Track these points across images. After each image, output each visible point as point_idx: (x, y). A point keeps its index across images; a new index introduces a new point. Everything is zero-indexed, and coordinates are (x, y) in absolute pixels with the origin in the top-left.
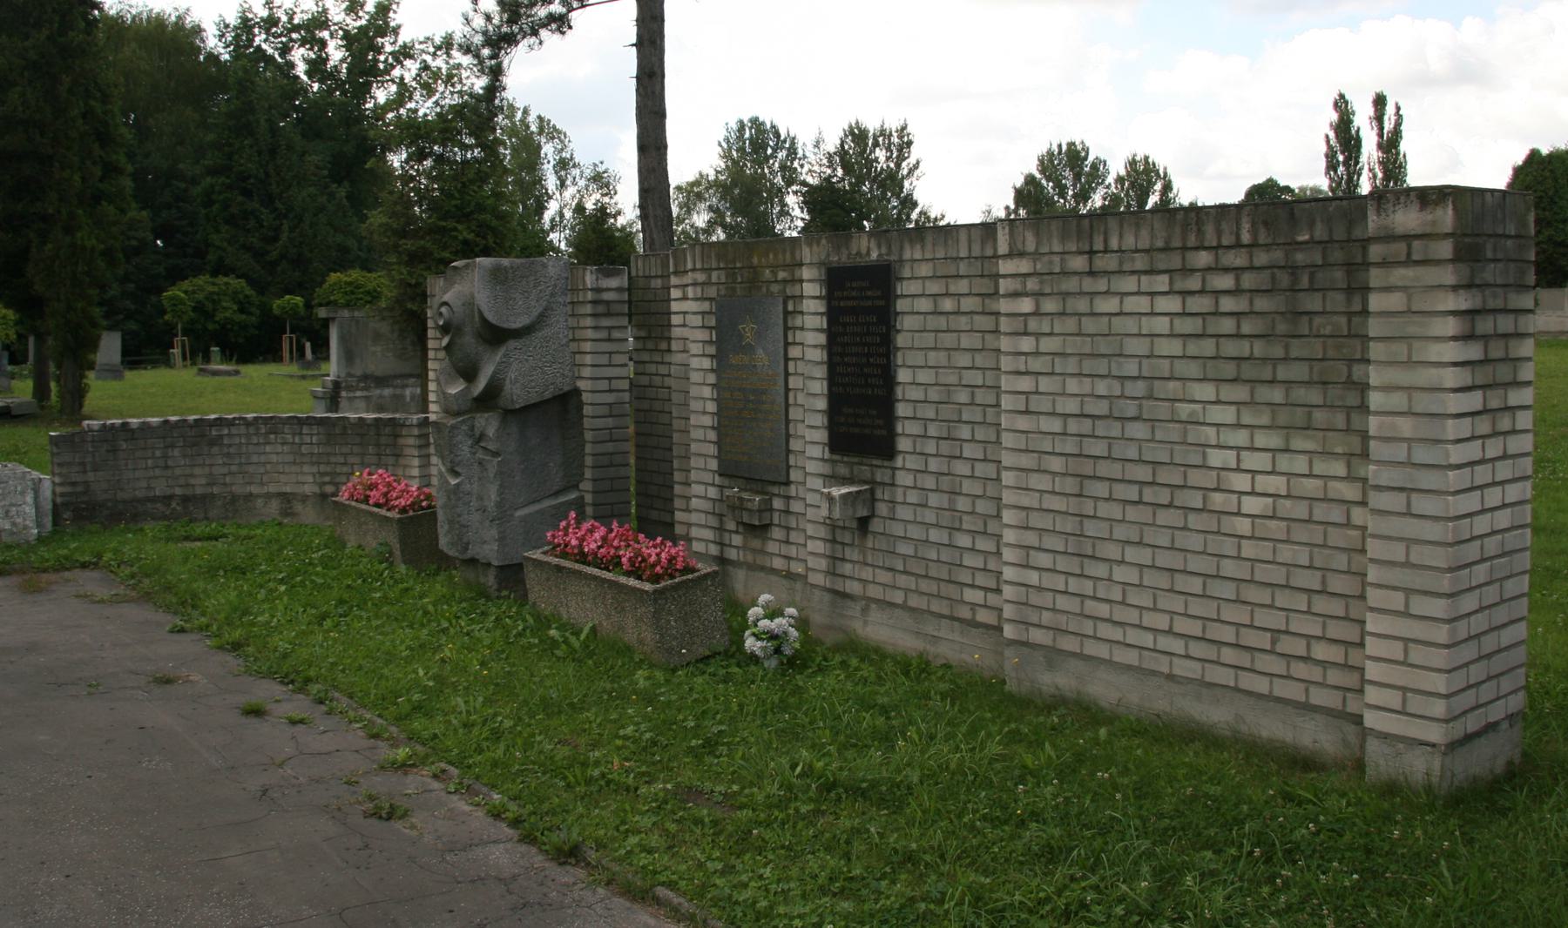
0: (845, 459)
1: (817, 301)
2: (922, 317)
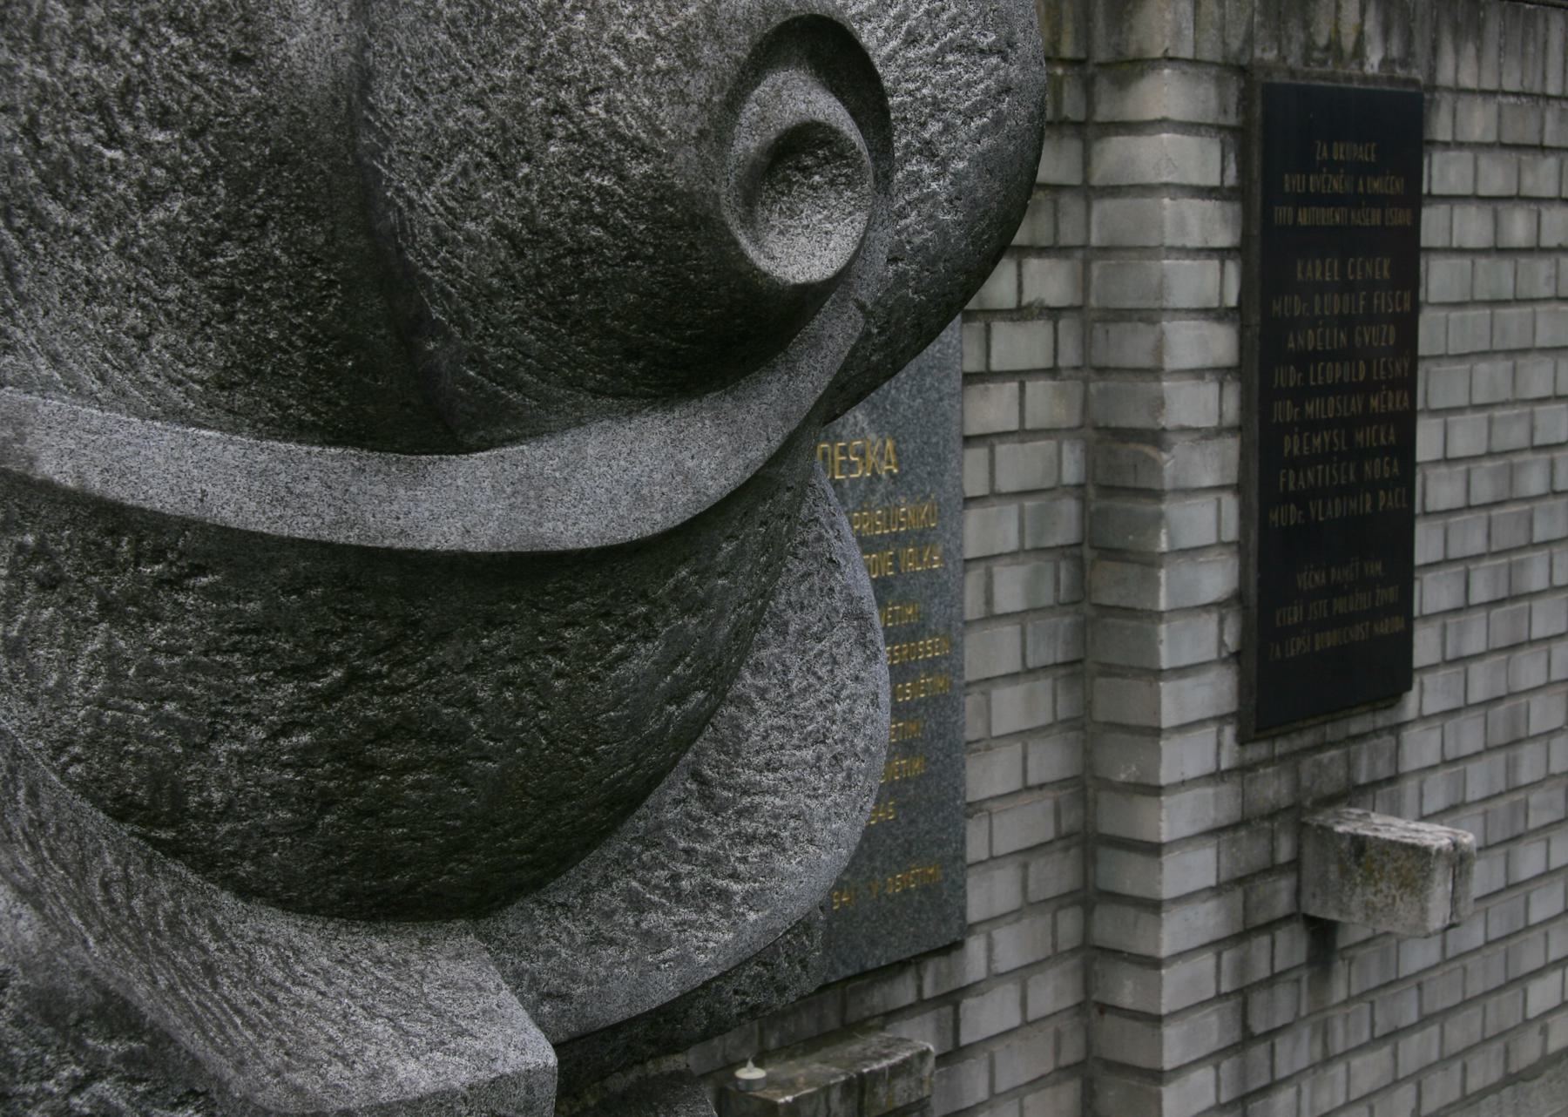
0: (1281, 747)
1: (1210, 206)
2: (1466, 262)
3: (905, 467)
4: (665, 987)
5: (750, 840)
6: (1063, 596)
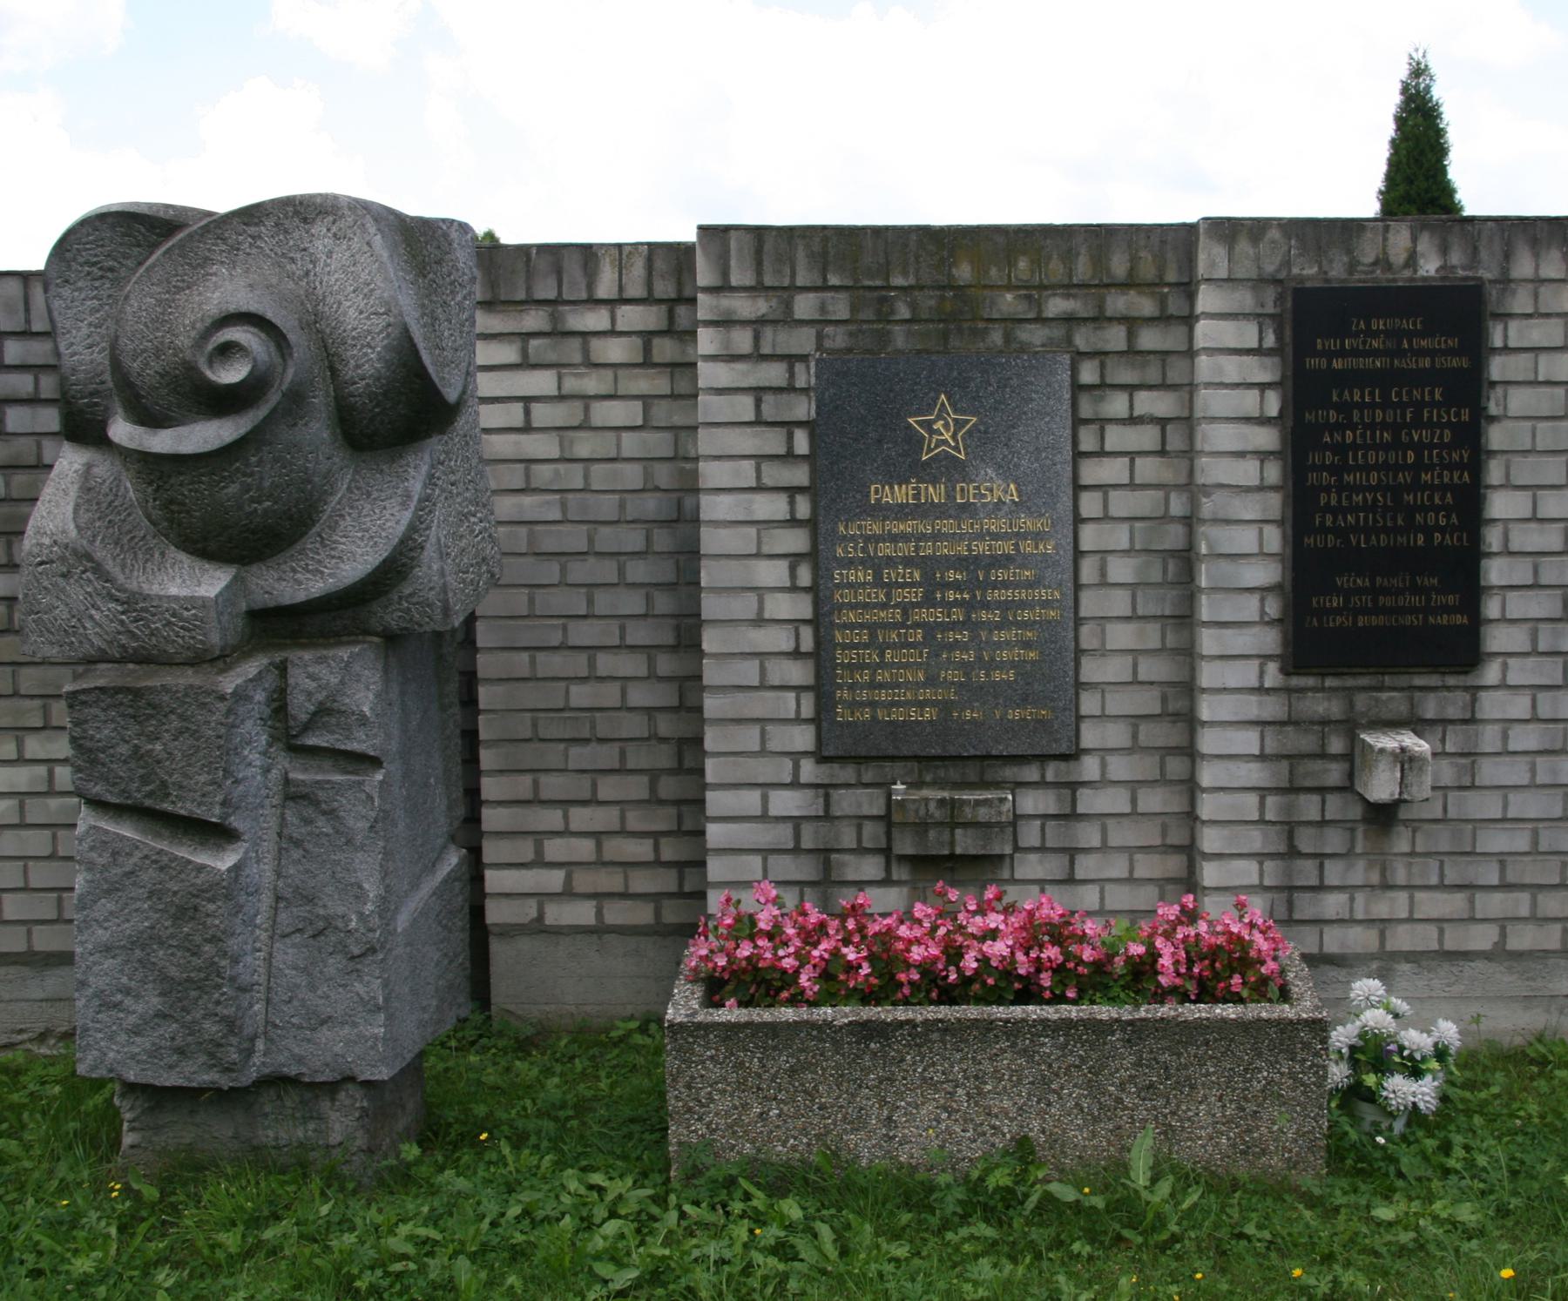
0: (1330, 682)
3: (1024, 498)
4: (301, 596)
5: (333, 557)
6: (1170, 577)
